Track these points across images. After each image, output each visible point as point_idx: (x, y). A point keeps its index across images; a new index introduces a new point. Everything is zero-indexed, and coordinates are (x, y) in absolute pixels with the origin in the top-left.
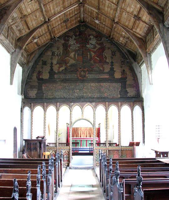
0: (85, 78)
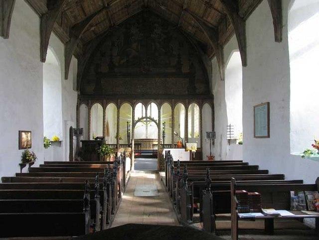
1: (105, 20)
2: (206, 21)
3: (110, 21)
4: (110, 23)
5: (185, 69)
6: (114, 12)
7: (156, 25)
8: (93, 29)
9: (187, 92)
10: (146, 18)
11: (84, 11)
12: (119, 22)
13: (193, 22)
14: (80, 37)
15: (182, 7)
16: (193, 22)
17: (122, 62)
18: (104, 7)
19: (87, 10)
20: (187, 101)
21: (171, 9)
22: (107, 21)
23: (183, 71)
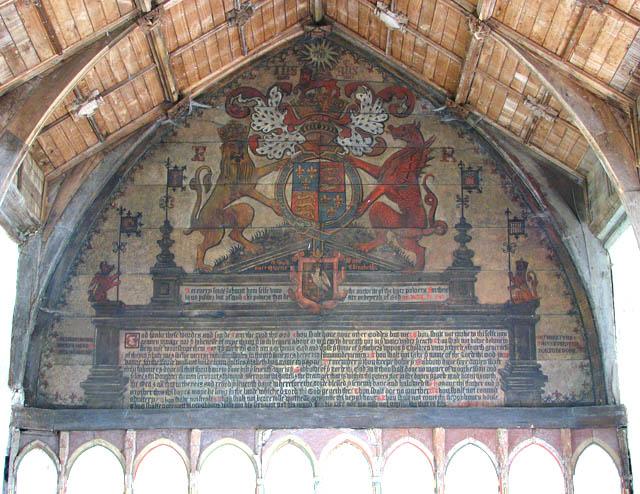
0: (328, 304)
1: (141, 69)
2: (582, 70)
3: (161, 76)
4: (164, 86)
5: (492, 289)
6: (183, 37)
7: (363, 97)
8: (88, 109)
9: (501, 396)
10: (315, 71)
11: (50, 31)
12: (199, 86)
13: (521, 78)
14: (29, 141)
15: (475, 14)
16: (521, 78)
17: (213, 256)
18: (139, 17)
19: (63, 24)
20: (503, 435)
21: (424, 27)
22: (150, 76)
23: (483, 299)
